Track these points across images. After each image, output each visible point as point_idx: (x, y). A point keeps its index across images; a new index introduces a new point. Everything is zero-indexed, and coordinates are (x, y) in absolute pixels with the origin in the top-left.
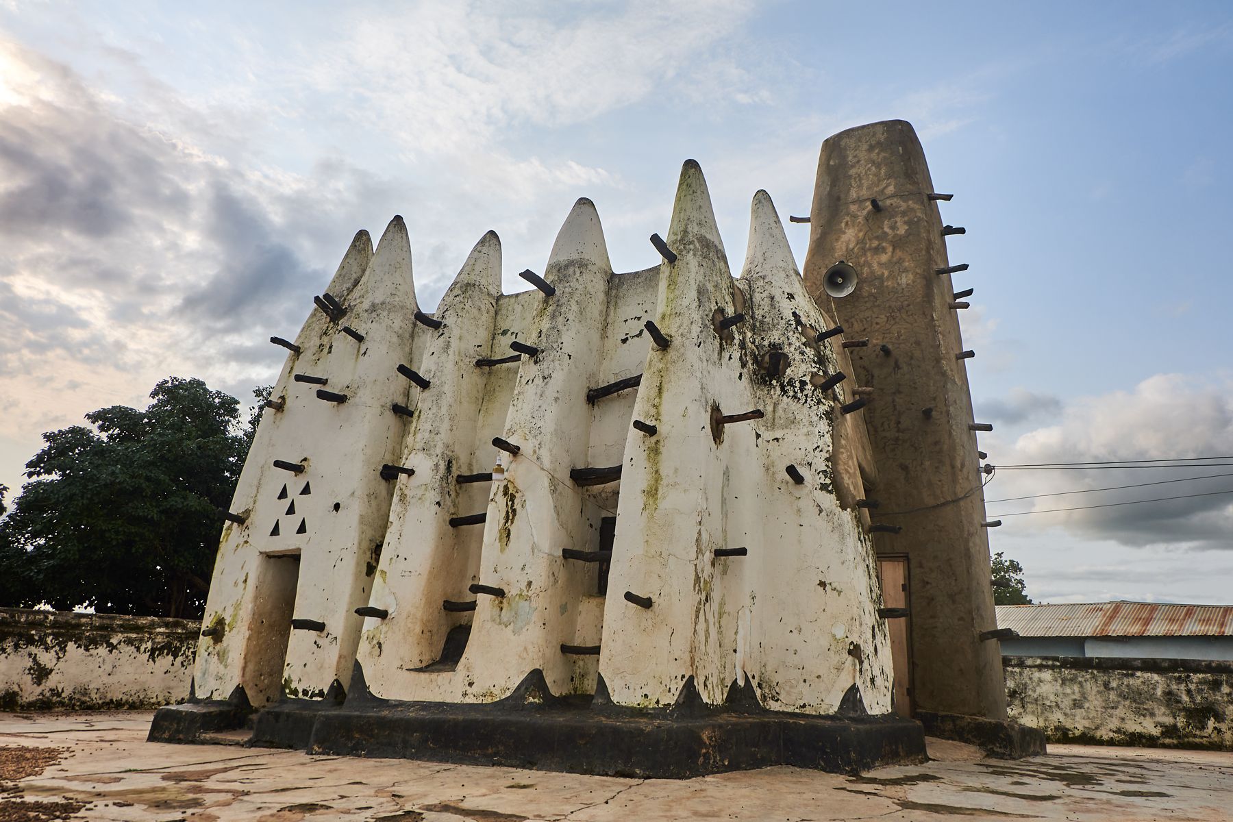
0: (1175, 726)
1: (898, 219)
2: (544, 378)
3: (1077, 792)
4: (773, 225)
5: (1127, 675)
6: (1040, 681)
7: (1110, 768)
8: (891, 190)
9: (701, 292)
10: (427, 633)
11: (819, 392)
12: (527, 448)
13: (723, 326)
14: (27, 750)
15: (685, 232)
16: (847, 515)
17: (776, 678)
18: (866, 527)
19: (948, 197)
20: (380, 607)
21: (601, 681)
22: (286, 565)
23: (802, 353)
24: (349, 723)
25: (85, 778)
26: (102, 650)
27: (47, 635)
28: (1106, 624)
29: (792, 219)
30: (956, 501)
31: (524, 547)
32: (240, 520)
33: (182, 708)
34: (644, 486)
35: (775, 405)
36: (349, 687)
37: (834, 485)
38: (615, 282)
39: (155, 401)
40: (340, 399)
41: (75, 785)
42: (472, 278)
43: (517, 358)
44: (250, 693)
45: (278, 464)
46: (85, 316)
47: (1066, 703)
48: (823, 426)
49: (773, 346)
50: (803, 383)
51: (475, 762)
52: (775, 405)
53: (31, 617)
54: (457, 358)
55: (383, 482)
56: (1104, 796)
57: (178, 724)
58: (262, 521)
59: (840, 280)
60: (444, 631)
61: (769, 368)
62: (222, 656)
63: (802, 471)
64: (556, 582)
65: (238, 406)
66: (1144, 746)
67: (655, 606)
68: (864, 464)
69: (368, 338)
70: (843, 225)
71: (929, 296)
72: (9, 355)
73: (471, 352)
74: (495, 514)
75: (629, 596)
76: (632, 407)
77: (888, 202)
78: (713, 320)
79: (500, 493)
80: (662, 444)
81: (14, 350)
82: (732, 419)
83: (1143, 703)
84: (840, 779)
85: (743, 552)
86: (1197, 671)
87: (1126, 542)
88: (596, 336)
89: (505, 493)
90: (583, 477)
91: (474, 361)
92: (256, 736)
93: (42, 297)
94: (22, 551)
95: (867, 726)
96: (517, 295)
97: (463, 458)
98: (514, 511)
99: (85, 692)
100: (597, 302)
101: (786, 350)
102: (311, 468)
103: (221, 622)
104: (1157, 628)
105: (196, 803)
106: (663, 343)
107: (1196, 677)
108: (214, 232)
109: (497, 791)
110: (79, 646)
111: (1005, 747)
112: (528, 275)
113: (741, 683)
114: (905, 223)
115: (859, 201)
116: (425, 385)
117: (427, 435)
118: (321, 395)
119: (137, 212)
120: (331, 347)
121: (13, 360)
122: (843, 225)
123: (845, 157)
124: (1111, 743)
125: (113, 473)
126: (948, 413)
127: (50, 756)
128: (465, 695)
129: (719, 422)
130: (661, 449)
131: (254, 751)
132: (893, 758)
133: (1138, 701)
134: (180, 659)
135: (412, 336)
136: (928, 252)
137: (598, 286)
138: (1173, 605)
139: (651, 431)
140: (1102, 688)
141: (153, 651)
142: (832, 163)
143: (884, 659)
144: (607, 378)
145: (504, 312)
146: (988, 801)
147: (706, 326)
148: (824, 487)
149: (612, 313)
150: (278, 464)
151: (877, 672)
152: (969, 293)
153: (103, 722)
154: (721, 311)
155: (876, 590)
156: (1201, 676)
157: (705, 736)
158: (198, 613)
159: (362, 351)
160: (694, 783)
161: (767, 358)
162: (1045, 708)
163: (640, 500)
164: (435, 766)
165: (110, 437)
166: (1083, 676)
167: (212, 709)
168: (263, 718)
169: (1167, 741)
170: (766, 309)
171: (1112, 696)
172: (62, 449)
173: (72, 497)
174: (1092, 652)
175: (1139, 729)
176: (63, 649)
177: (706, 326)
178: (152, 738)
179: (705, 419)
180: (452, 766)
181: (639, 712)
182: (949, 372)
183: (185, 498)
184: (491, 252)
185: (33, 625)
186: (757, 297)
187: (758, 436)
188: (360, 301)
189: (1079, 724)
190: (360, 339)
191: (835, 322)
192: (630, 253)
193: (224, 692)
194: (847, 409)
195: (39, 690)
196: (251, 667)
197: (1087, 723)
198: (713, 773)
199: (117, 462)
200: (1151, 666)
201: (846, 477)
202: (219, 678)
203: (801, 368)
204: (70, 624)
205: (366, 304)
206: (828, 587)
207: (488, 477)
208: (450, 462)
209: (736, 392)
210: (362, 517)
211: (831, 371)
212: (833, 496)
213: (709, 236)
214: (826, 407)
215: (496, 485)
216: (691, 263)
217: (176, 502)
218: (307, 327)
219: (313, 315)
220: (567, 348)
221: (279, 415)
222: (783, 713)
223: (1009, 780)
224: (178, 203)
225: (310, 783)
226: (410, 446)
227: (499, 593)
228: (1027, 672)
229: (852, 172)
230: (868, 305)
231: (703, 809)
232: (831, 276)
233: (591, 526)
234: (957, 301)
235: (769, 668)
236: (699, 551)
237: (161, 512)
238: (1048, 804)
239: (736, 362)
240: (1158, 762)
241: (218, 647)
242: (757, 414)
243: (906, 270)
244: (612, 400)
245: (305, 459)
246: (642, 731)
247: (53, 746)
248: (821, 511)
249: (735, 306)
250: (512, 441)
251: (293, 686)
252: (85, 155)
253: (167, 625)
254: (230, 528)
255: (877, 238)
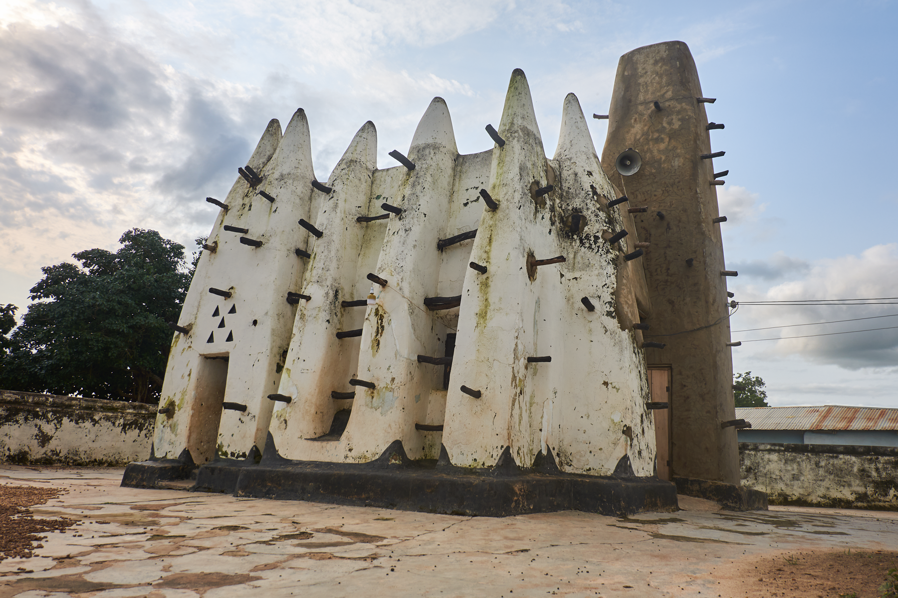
0: (866, 494)
1: (674, 117)
2: (406, 231)
3: (782, 531)
4: (579, 119)
5: (832, 457)
6: (769, 461)
7: (810, 519)
8: (669, 94)
9: (522, 169)
10: (320, 413)
11: (608, 245)
12: (392, 281)
13: (538, 194)
14: (35, 489)
15: (512, 123)
16: (625, 335)
17: (570, 450)
18: (640, 344)
19: (712, 101)
20: (286, 394)
21: (443, 449)
22: (218, 364)
23: (597, 216)
24: (263, 475)
25: (76, 507)
26: (88, 424)
27: (48, 412)
28: (821, 421)
29: (595, 116)
30: (708, 327)
31: (389, 353)
32: (186, 331)
33: (145, 464)
34: (477, 310)
35: (575, 253)
36: (265, 450)
37: (617, 313)
38: (459, 160)
39: (122, 246)
40: (257, 244)
41: (68, 511)
42: (355, 157)
43: (387, 216)
44: (194, 455)
45: (212, 291)
46: (72, 184)
47: (787, 477)
48: (610, 269)
49: (576, 211)
50: (596, 238)
51: (352, 503)
52: (575, 253)
53: (36, 399)
54: (343, 215)
55: (289, 305)
56: (801, 534)
57: (143, 475)
58: (201, 332)
59: (628, 163)
60: (332, 413)
61: (571, 226)
62: (173, 428)
63: (593, 302)
64: (412, 378)
65: (183, 250)
66: (843, 508)
67: (483, 396)
68: (641, 299)
69: (277, 200)
70: (633, 121)
71: (694, 176)
72: (15, 212)
73: (354, 211)
74: (368, 329)
75: (464, 389)
76: (469, 253)
77: (667, 104)
78: (530, 189)
79: (373, 314)
80: (490, 279)
81: (18, 209)
82: (542, 262)
83: (843, 477)
84: (613, 520)
85: (548, 359)
86: (884, 454)
87: (845, 366)
88: (444, 201)
89: (376, 314)
90: (434, 304)
91: (356, 218)
92: (198, 484)
93: (39, 169)
94: (28, 353)
95: (634, 484)
96: (388, 170)
97: (347, 289)
98: (383, 327)
99: (76, 453)
100: (446, 176)
101: (585, 213)
102: (236, 294)
103: (172, 404)
104: (857, 425)
105: (154, 523)
106: (493, 206)
107: (883, 459)
108: (189, 127)
109: (367, 522)
110: (71, 421)
111: (736, 502)
112: (395, 154)
113: (544, 452)
114: (679, 120)
115: (646, 103)
116: (319, 234)
117: (320, 271)
118: (244, 241)
119: (132, 110)
120: (250, 206)
121: (18, 215)
122: (633, 121)
123: (636, 69)
124: (818, 505)
125: (94, 298)
126: (705, 263)
127: (52, 493)
128: (346, 457)
129: (533, 265)
130: (490, 283)
131: (196, 494)
132: (652, 506)
133: (840, 476)
134: (144, 432)
135: (310, 199)
136: (695, 142)
137: (447, 164)
138: (871, 409)
139: (483, 270)
140: (814, 466)
141: (124, 426)
142: (626, 73)
143: (649, 439)
144: (452, 231)
145: (378, 182)
146: (716, 535)
147: (525, 194)
148: (609, 314)
149: (457, 184)
150: (212, 291)
151: (643, 447)
152: (725, 173)
153: (89, 474)
154: (537, 183)
155: (645, 389)
156: (886, 458)
157: (517, 488)
158: (156, 401)
159: (273, 209)
160: (507, 520)
161: (570, 219)
162: (771, 479)
163: (474, 320)
164: (324, 506)
165: (91, 272)
166: (801, 457)
167: (166, 465)
168: (202, 471)
169: (860, 504)
170: (571, 182)
171: (821, 472)
172: (56, 279)
173: (63, 315)
174: (809, 441)
175: (839, 496)
176: (60, 422)
177: (525, 194)
178: (124, 484)
179: (523, 262)
180: (336, 506)
181: (470, 471)
182: (707, 232)
183: (146, 317)
184: (369, 137)
185: (37, 404)
186: (565, 174)
187: (562, 276)
188: (272, 172)
189: (796, 492)
190: (272, 200)
191: (623, 194)
192: (471, 140)
193: (175, 453)
194: (628, 257)
195: (43, 450)
196: (194, 436)
197: (801, 491)
198: (521, 514)
199: (97, 290)
200: (851, 451)
201: (626, 308)
202: (171, 443)
203: (595, 226)
204: (64, 405)
205: (277, 175)
206: (610, 386)
207: (364, 303)
208: (337, 291)
209: (546, 243)
210: (273, 330)
211: (618, 229)
212: (616, 320)
213: (529, 127)
214: (613, 256)
215: (370, 309)
216: (516, 146)
217: (140, 320)
218: (234, 190)
219: (238, 182)
220: (423, 209)
221: (213, 255)
222: (574, 474)
223: (736, 523)
224: (162, 103)
225: (236, 514)
226: (308, 279)
227: (371, 386)
228: (760, 454)
229: (641, 80)
230: (649, 181)
231: (511, 535)
232: (621, 158)
233: (439, 339)
234: (715, 180)
235: (565, 443)
236: (516, 358)
237: (129, 327)
238: (760, 537)
239: (547, 221)
240: (848, 516)
241: (170, 422)
242: (561, 259)
243: (678, 156)
244: (456, 248)
245: (232, 288)
246: (471, 483)
247: (53, 487)
248: (606, 331)
249: (547, 179)
250: (382, 276)
251: (224, 449)
252: (97, 67)
253: (134, 408)
254: (178, 337)
255: (658, 131)
